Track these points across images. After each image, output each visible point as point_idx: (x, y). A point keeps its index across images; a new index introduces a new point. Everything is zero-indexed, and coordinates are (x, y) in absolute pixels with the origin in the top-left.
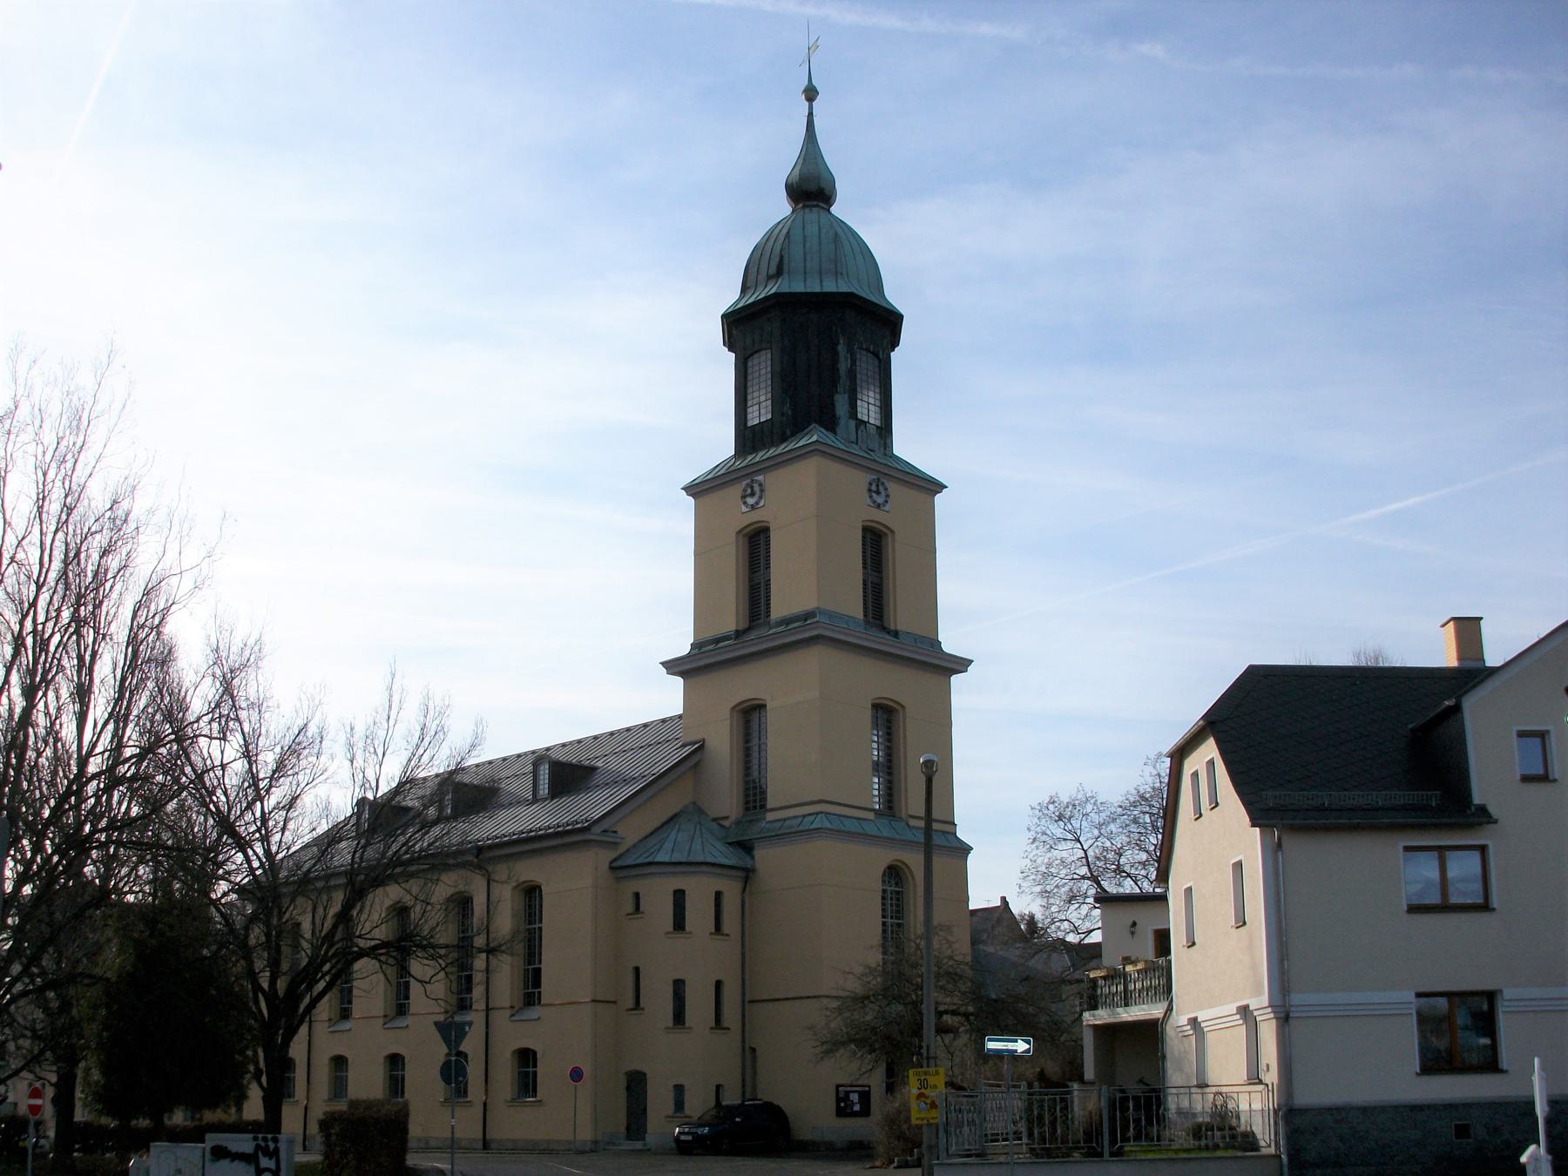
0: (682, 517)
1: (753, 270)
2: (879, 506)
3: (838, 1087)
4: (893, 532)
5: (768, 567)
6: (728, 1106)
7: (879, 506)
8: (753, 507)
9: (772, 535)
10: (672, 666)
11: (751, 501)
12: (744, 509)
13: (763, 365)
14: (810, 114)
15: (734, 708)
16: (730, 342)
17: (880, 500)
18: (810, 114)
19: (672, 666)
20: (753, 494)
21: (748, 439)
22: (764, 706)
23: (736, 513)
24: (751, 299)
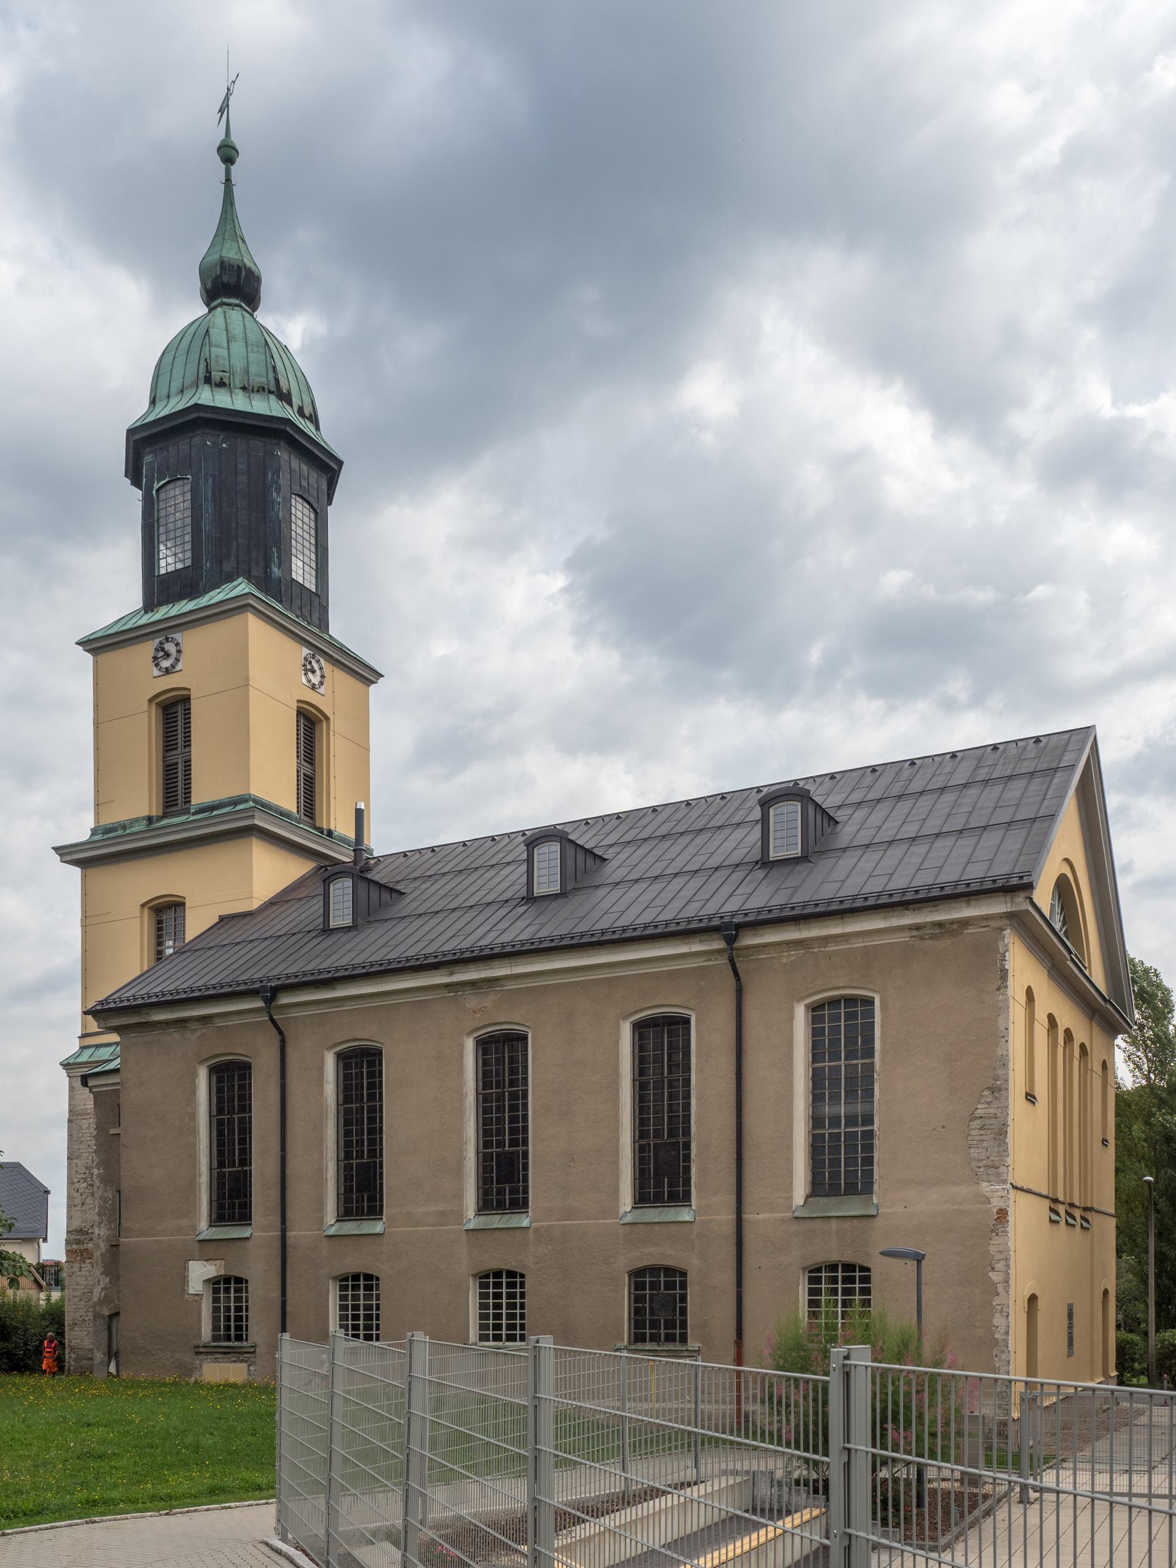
0: (77, 677)
1: (166, 368)
2: (313, 687)
3: (522, 1276)
4: (327, 719)
5: (187, 744)
6: (186, 1268)
7: (313, 687)
8: (167, 671)
9: (194, 704)
10: (66, 853)
11: (166, 664)
12: (156, 672)
13: (178, 501)
14: (228, 180)
15: (151, 700)
16: (134, 473)
17: (315, 680)
18: (228, 180)
19: (66, 853)
20: (167, 655)
21: (159, 589)
22: (183, 904)
23: (141, 673)
24: (163, 410)
